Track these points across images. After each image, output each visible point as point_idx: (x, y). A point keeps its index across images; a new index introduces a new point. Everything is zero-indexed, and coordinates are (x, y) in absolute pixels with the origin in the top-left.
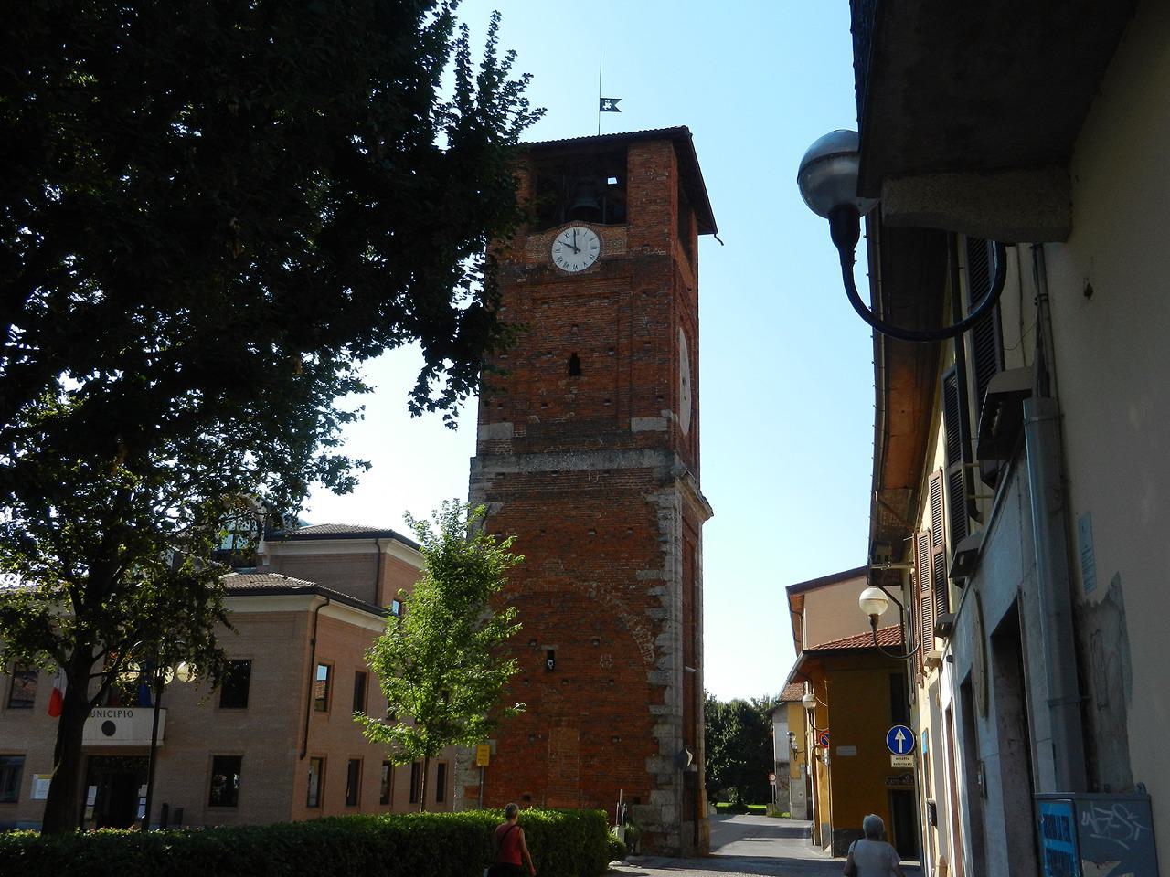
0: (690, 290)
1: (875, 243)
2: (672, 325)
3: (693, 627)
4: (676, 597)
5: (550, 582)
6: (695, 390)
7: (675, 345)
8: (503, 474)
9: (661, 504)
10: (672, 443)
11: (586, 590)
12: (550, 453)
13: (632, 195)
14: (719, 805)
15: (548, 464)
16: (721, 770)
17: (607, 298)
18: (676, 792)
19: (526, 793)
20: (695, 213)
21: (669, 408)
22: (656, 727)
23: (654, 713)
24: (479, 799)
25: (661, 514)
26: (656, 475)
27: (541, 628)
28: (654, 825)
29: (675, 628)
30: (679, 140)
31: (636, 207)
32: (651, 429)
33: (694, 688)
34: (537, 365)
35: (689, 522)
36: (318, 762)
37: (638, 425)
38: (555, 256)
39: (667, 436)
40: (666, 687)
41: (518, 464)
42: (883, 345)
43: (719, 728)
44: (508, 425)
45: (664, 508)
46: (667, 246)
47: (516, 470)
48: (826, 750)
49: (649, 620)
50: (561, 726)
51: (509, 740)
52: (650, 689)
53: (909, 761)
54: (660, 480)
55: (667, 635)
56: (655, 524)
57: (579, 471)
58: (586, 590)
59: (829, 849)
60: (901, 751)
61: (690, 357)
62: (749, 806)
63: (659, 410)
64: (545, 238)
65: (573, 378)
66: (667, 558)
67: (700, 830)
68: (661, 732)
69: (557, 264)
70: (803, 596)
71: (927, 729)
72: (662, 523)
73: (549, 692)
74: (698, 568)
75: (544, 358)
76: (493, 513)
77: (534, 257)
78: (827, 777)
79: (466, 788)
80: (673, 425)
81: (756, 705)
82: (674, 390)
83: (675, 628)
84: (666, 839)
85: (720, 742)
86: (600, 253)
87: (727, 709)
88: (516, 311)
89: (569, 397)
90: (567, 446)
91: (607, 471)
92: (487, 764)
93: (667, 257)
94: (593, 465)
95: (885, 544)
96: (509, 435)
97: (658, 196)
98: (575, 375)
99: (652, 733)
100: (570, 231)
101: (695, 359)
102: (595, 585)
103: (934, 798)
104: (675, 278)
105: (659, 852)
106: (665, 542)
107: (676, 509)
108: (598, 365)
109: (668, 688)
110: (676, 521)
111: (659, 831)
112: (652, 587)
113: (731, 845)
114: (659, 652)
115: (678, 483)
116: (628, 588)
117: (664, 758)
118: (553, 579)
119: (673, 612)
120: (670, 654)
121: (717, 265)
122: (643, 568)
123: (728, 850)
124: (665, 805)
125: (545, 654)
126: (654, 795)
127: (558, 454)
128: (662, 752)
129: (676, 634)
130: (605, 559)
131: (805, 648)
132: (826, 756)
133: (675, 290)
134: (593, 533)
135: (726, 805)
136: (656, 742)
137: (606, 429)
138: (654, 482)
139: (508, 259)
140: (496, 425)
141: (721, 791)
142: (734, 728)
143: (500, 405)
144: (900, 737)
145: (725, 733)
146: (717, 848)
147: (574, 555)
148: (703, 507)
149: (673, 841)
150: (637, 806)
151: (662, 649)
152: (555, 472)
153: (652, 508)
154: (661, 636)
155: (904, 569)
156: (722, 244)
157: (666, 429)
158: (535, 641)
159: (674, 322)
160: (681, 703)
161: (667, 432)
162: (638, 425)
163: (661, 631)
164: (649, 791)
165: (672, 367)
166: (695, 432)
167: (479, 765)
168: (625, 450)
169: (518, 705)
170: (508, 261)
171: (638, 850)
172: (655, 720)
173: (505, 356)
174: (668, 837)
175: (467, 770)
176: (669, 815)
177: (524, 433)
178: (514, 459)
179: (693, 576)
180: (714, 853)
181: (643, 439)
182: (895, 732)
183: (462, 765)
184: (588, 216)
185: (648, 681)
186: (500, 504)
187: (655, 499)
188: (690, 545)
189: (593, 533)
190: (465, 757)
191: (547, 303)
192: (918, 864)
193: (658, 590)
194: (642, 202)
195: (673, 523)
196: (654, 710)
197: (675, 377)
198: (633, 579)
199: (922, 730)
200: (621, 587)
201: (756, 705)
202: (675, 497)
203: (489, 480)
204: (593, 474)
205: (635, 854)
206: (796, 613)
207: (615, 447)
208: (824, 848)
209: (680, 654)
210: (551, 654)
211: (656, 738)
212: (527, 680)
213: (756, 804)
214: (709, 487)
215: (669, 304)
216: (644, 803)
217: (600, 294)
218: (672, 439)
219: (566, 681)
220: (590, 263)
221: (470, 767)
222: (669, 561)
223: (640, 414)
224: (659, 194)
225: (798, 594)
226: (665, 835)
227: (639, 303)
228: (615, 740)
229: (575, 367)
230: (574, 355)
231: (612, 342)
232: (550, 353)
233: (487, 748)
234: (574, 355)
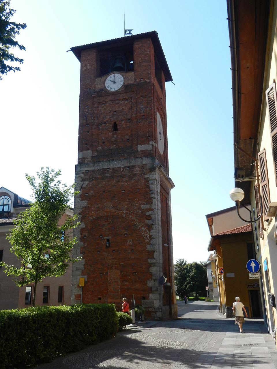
0: (161, 98)
1: (232, 21)
2: (153, 109)
3: (168, 229)
4: (158, 215)
5: (108, 212)
6: (165, 138)
7: (154, 117)
8: (88, 171)
9: (150, 178)
10: (154, 154)
11: (121, 214)
12: (106, 161)
13: (136, 60)
14: (190, 298)
15: (105, 165)
16: (190, 286)
17: (127, 100)
18: (160, 294)
19: (99, 297)
20: (163, 73)
21: (153, 141)
22: (151, 268)
23: (150, 262)
24: (80, 300)
25: (150, 182)
26: (148, 167)
27: (104, 230)
28: (151, 308)
29: (158, 227)
30: (152, 37)
31: (137, 64)
32: (145, 149)
33: (168, 253)
34: (101, 128)
35: (164, 188)
36: (47, 287)
37: (140, 148)
38: (106, 85)
39: (152, 152)
40: (154, 251)
41: (94, 166)
42: (235, 50)
43: (189, 272)
44: (90, 152)
45: (152, 180)
46: (150, 78)
47: (93, 169)
48: (222, 275)
49: (147, 225)
50: (112, 269)
51: (92, 276)
52: (148, 253)
53: (258, 276)
54: (150, 169)
55: (154, 231)
56: (148, 187)
57: (117, 167)
58: (121, 214)
59: (225, 314)
60: (253, 271)
61: (163, 125)
62: (200, 298)
63: (149, 141)
64: (102, 79)
65: (115, 132)
66: (154, 200)
67: (172, 309)
68: (153, 270)
69: (107, 88)
70: (212, 219)
71: (267, 258)
72: (151, 186)
73: (108, 256)
74: (169, 206)
75: (103, 125)
76: (84, 186)
77: (98, 87)
78: (223, 286)
79: (76, 296)
80: (155, 149)
81: (201, 264)
82: (155, 134)
83: (158, 227)
84: (156, 314)
85: (189, 276)
86: (124, 83)
87: (191, 265)
88: (92, 107)
89: (113, 139)
90: (113, 158)
91: (129, 167)
92: (83, 285)
93: (150, 82)
94: (123, 165)
95: (241, 169)
96: (90, 155)
97: (146, 59)
98: (115, 131)
99: (149, 270)
100: (112, 76)
101: (165, 126)
102: (125, 212)
103: (273, 292)
104: (154, 92)
105: (153, 319)
106: (152, 193)
107: (157, 180)
108: (124, 126)
109: (155, 252)
110: (157, 185)
111: (153, 310)
112: (148, 211)
113: (188, 314)
114: (151, 237)
115: (157, 169)
116: (138, 212)
117: (155, 280)
118: (108, 210)
119: (157, 221)
120: (156, 238)
121: (176, 96)
122: (144, 204)
123: (186, 316)
124: (155, 300)
125: (106, 240)
126: (151, 296)
127: (109, 161)
128: (154, 278)
129: (158, 230)
130: (128, 201)
131: (214, 235)
132: (222, 277)
133: (154, 95)
134: (124, 191)
135: (192, 298)
136: (151, 274)
137: (127, 150)
138: (147, 170)
139: (89, 88)
140: (85, 152)
141: (190, 293)
142: (193, 272)
143: (87, 144)
144: (253, 265)
145: (190, 273)
146: (182, 315)
147: (116, 201)
148: (170, 182)
149: (159, 314)
150: (144, 300)
151: (152, 236)
152: (108, 168)
153: (147, 180)
154: (152, 231)
155: (253, 181)
156: (175, 85)
157: (151, 149)
158: (102, 235)
159: (154, 108)
160: (161, 258)
161: (152, 150)
162: (140, 148)
163: (152, 229)
164: (148, 294)
165: (153, 125)
166: (166, 154)
167: (80, 286)
168: (136, 158)
169: (78, 257)
170: (88, 89)
171: (143, 319)
172: (150, 265)
173: (88, 125)
174: (157, 313)
175: (76, 288)
176: (157, 303)
177: (96, 154)
178: (92, 165)
179: (167, 209)
180: (180, 318)
181: (142, 153)
182: (250, 263)
183: (74, 286)
184: (119, 70)
185: (147, 249)
186: (87, 182)
187: (148, 176)
188: (165, 197)
189: (124, 191)
190: (75, 283)
191: (104, 104)
192: (263, 320)
193: (150, 213)
194: (140, 62)
195: (156, 186)
196: (150, 261)
197: (155, 129)
198: (140, 209)
199: (263, 259)
200: (135, 212)
201: (201, 264)
202: (157, 175)
203: (83, 173)
204: (123, 168)
205: (142, 321)
206: (210, 226)
207: (132, 157)
208: (224, 314)
209: (161, 239)
210: (108, 240)
211: (151, 272)
212: (99, 251)
213: (203, 297)
214: (172, 174)
215: (151, 100)
216: (147, 299)
217: (124, 99)
218: (154, 153)
219: (114, 251)
220: (120, 87)
221: (77, 287)
222: (154, 201)
223: (141, 144)
224: (146, 58)
225: (210, 217)
226: (155, 312)
227: (139, 101)
228: (134, 274)
229: (115, 127)
230: (115, 123)
231: (129, 117)
232: (105, 123)
233: (84, 279)
234: (115, 123)
